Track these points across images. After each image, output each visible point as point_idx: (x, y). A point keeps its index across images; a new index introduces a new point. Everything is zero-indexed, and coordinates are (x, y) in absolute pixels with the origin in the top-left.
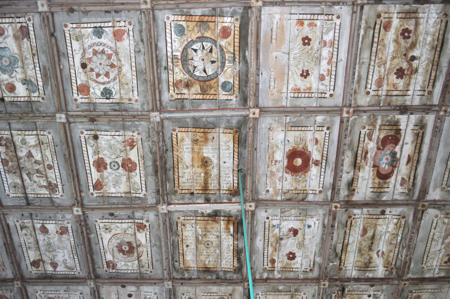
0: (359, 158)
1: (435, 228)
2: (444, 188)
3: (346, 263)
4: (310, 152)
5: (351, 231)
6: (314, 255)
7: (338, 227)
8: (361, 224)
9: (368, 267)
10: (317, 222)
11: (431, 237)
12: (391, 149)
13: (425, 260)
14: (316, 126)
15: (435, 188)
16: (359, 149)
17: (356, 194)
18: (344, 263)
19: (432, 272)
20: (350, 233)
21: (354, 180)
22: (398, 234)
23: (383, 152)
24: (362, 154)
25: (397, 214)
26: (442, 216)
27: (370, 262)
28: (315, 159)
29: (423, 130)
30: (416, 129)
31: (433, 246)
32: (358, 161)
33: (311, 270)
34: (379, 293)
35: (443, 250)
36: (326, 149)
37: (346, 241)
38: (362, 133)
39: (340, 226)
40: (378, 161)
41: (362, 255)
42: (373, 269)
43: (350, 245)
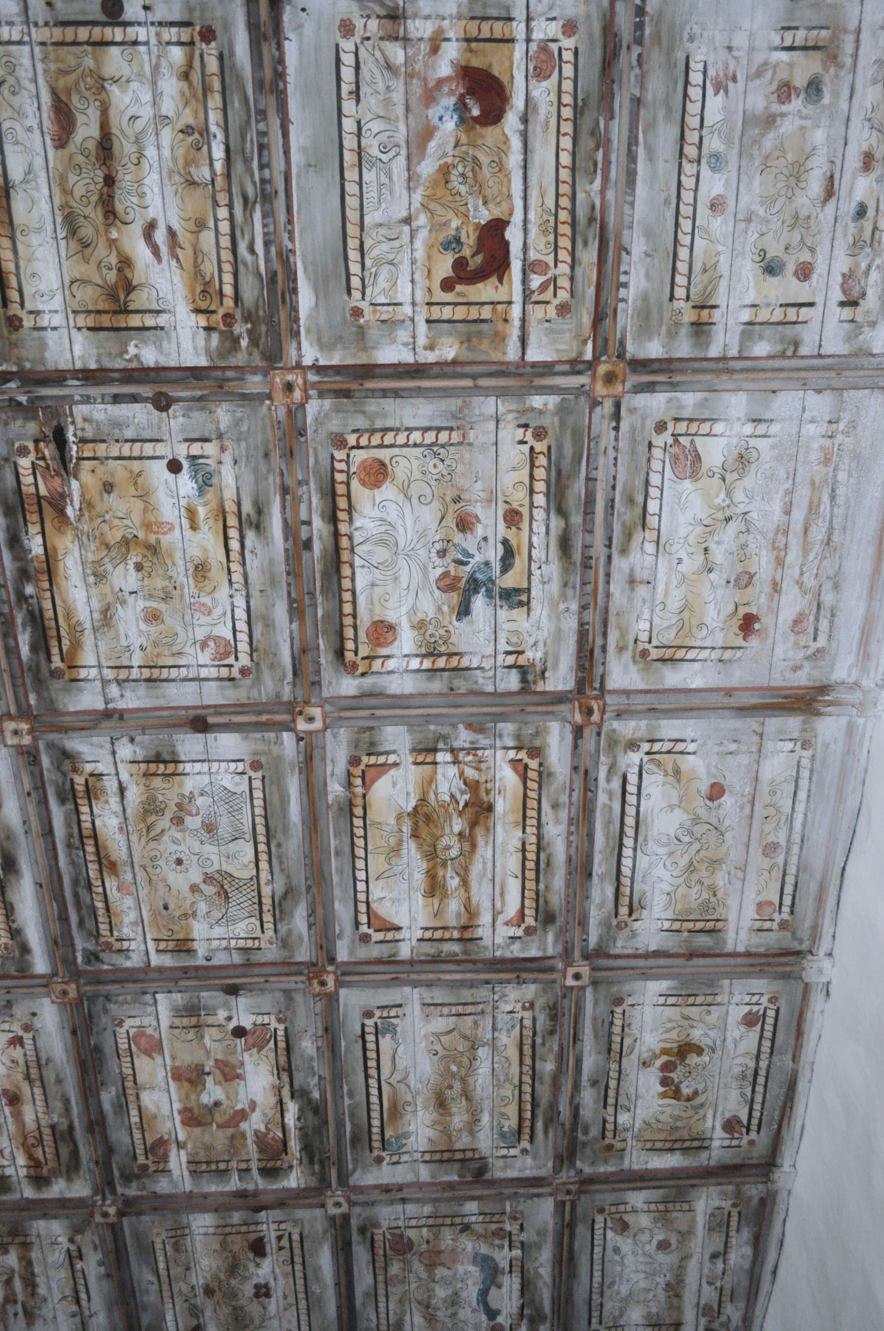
1: (356, 94)
3: (28, 291)
9: (126, 311)
11: (350, 142)
13: (355, 268)
19: (403, 335)
31: (371, 195)
34: (210, 449)
35: (422, 219)
41: (85, 245)
42: (150, 321)
43: (21, 194)
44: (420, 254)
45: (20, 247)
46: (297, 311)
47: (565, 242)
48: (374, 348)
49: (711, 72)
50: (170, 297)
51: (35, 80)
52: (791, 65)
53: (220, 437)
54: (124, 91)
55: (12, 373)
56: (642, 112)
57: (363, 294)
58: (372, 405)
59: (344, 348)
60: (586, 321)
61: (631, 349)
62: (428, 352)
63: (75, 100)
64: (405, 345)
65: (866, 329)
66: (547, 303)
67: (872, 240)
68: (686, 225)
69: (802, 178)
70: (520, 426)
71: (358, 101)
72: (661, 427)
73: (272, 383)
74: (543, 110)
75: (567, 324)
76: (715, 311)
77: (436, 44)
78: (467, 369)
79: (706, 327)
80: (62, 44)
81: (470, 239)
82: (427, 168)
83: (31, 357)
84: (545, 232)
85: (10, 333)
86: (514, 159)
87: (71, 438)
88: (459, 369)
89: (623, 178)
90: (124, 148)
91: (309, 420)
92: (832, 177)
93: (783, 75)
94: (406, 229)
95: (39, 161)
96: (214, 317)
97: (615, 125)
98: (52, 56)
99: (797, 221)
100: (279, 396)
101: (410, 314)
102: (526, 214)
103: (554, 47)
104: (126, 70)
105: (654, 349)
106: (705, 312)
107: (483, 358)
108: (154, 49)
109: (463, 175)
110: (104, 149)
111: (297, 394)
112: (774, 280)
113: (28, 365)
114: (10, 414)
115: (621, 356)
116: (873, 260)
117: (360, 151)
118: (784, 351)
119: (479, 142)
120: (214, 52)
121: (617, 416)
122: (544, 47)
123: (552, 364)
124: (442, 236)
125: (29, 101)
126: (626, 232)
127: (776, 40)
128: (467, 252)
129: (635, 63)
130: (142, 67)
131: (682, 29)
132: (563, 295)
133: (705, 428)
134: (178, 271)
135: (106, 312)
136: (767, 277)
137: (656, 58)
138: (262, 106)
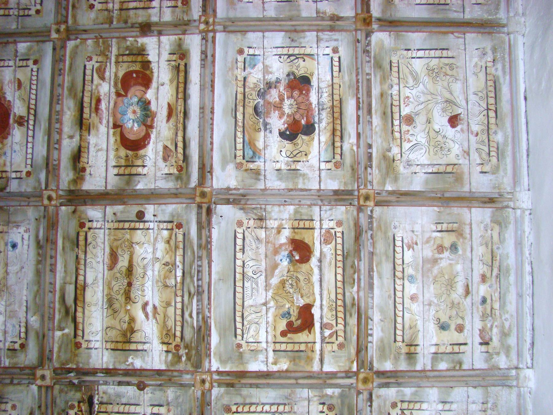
0: (86, 111)
1: (243, 250)
2: (241, 164)
4: (9, 101)
5: (88, 256)
6: (25, 308)
7: (64, 248)
8: (106, 243)
9: (130, 342)
10: (26, 236)
11: (239, 270)
12: (139, 94)
13: (239, 325)
14: (18, 59)
15: (224, 163)
16: (86, 94)
17: (88, 177)
18: (83, 331)
19: (261, 357)
20: (85, 260)
21: (82, 150)
22: (175, 264)
23: (126, 100)
24: (91, 103)
25: (167, 219)
26: (252, 222)
27: (133, 331)
28: (17, 114)
29: (184, 60)
30: (174, 59)
31: (248, 292)
32: (85, 116)
33: (23, 346)
35: (272, 304)
36: (33, 97)
37: (81, 278)
38: (87, 67)
39: (68, 245)
40: (119, 116)
42: (140, 347)
43: (90, 288)
44: (271, 319)
45: (86, 311)
46: (210, 345)
47: (341, 315)
48: (247, 363)
49: (405, 241)
50: (151, 336)
51: (104, 243)
52: (442, 238)
53: (168, 404)
54: (141, 248)
55: (73, 369)
56: (375, 257)
57: (243, 337)
58: (245, 391)
59: (232, 363)
60: (353, 351)
61: (376, 366)
62: (274, 366)
63: (120, 252)
64: (263, 362)
65: (495, 356)
66: (333, 343)
67: (491, 313)
68: (400, 307)
69: (453, 286)
70: (320, 404)
71: (243, 253)
72: (394, 405)
73: (195, 379)
74: (328, 257)
75: (343, 353)
76: (417, 347)
77: (279, 230)
78: (293, 375)
79: (414, 355)
80: (118, 229)
81: (294, 313)
82: (275, 281)
83: (83, 361)
84: (331, 310)
85: (75, 350)
86: (316, 278)
87: (96, 401)
88: (289, 374)
89: (367, 287)
90: (138, 271)
91: (213, 398)
92: (468, 285)
93: (438, 242)
94: (264, 308)
95: (100, 276)
96: (170, 346)
97: (362, 263)
98: (113, 233)
99: (453, 305)
100: (198, 385)
101: (265, 347)
102: (321, 301)
103: (333, 231)
104: (143, 239)
105: (388, 366)
106: (413, 348)
107: (300, 369)
108: (156, 231)
109: (291, 284)
110: (129, 271)
111: (207, 385)
112: (446, 333)
113: (81, 365)
114: (69, 388)
115: (371, 369)
116: (493, 323)
117: (243, 274)
118: (454, 367)
119: (299, 270)
120: (181, 233)
121: (370, 399)
122: (328, 231)
123: (336, 373)
124: (281, 312)
125: (100, 251)
126: (370, 310)
127: (434, 228)
128: (293, 319)
129: (369, 238)
130: (150, 238)
131: (390, 224)
132: (341, 339)
133: (417, 406)
134: (156, 325)
135: (121, 342)
136: (442, 331)
137: (379, 236)
138: (200, 255)
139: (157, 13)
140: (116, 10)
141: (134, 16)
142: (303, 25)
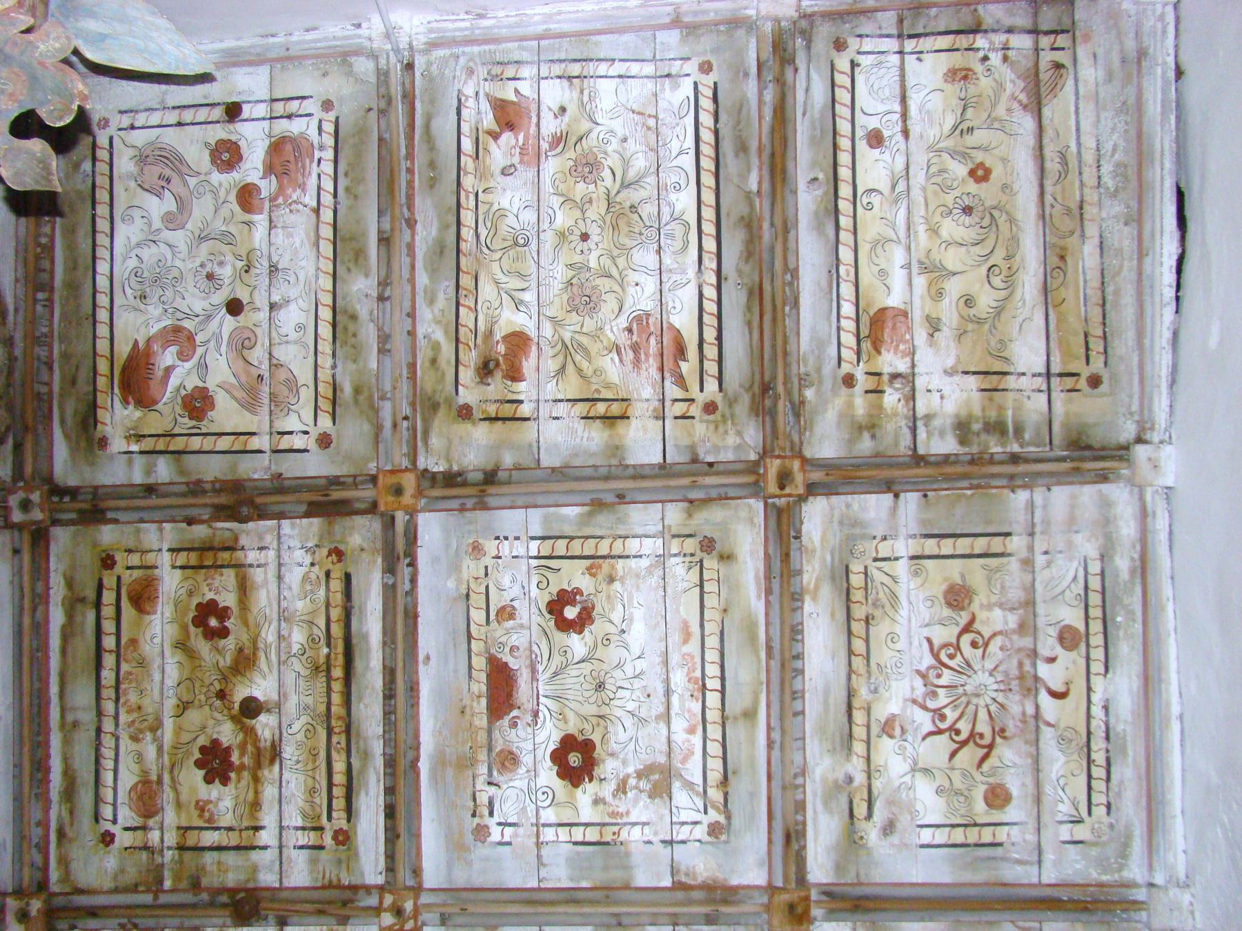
139: (273, 862)
140: (169, 848)
141: (215, 867)
142: (638, 914)
